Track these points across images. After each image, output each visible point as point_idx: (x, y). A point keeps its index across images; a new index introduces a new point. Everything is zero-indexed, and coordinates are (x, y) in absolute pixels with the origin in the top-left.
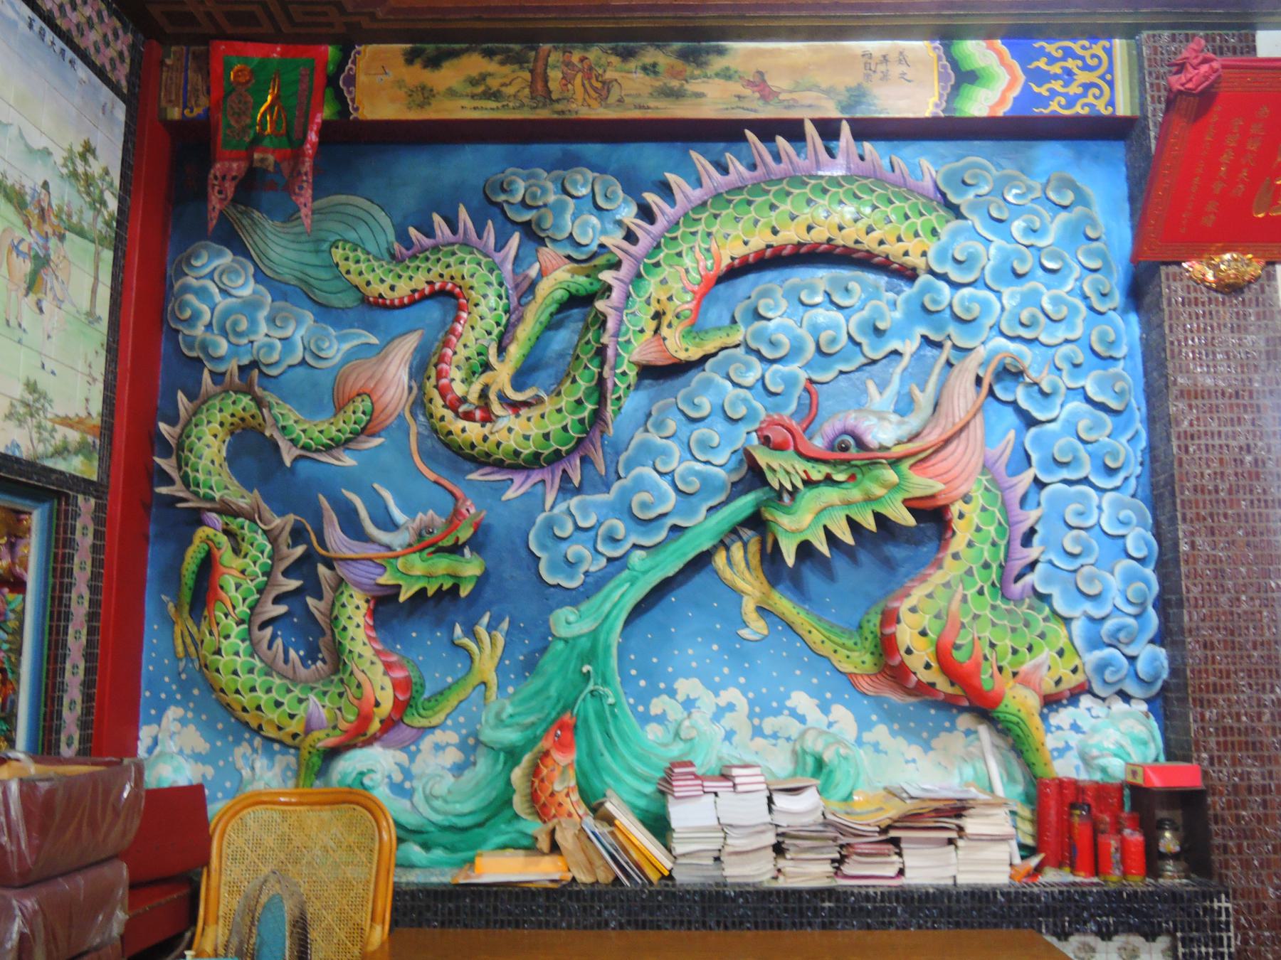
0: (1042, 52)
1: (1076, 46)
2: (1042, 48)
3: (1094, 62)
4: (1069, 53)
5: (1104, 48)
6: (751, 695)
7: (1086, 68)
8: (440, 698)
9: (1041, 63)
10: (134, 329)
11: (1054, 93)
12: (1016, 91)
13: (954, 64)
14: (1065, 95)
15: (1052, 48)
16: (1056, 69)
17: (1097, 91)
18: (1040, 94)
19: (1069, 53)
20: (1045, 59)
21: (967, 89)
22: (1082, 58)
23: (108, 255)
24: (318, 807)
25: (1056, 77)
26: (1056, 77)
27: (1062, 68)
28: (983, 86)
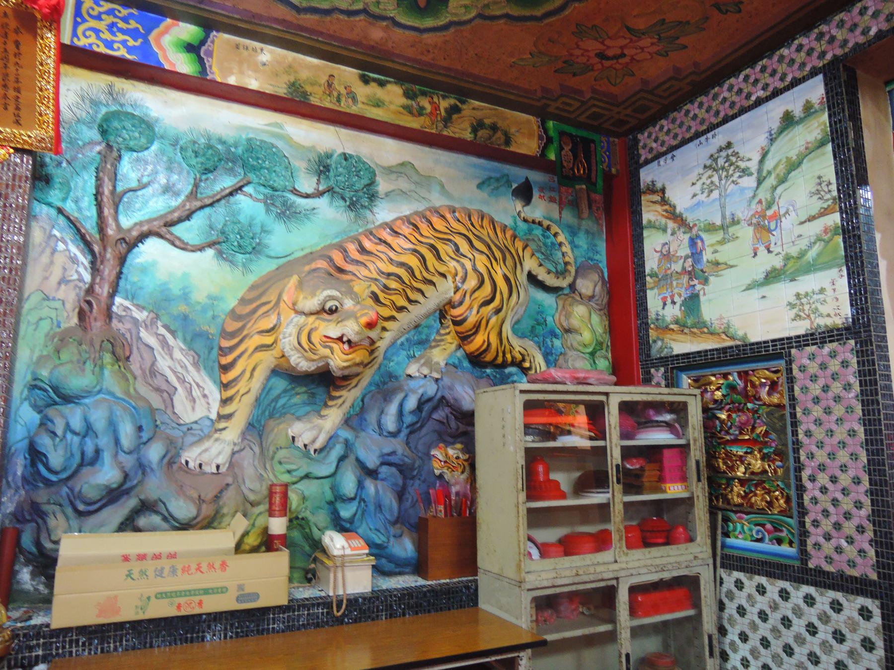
0: (130, 50)
1: (102, 49)
2: (128, 53)
3: (88, 33)
4: (109, 44)
5: (79, 39)
6: (204, 617)
7: (97, 31)
8: (537, 221)
9: (131, 43)
10: (632, 345)
11: (125, 20)
12: (155, 32)
13: (201, 61)
14: (116, 16)
15: (122, 53)
16: (120, 37)
17: (91, 12)
18: (137, 22)
19: (109, 44)
20: (129, 44)
21: (196, 43)
22: (98, 37)
23: (844, 269)
24: (78, 237)
25: (121, 30)
26: (121, 30)
27: (116, 36)
28: (184, 42)
